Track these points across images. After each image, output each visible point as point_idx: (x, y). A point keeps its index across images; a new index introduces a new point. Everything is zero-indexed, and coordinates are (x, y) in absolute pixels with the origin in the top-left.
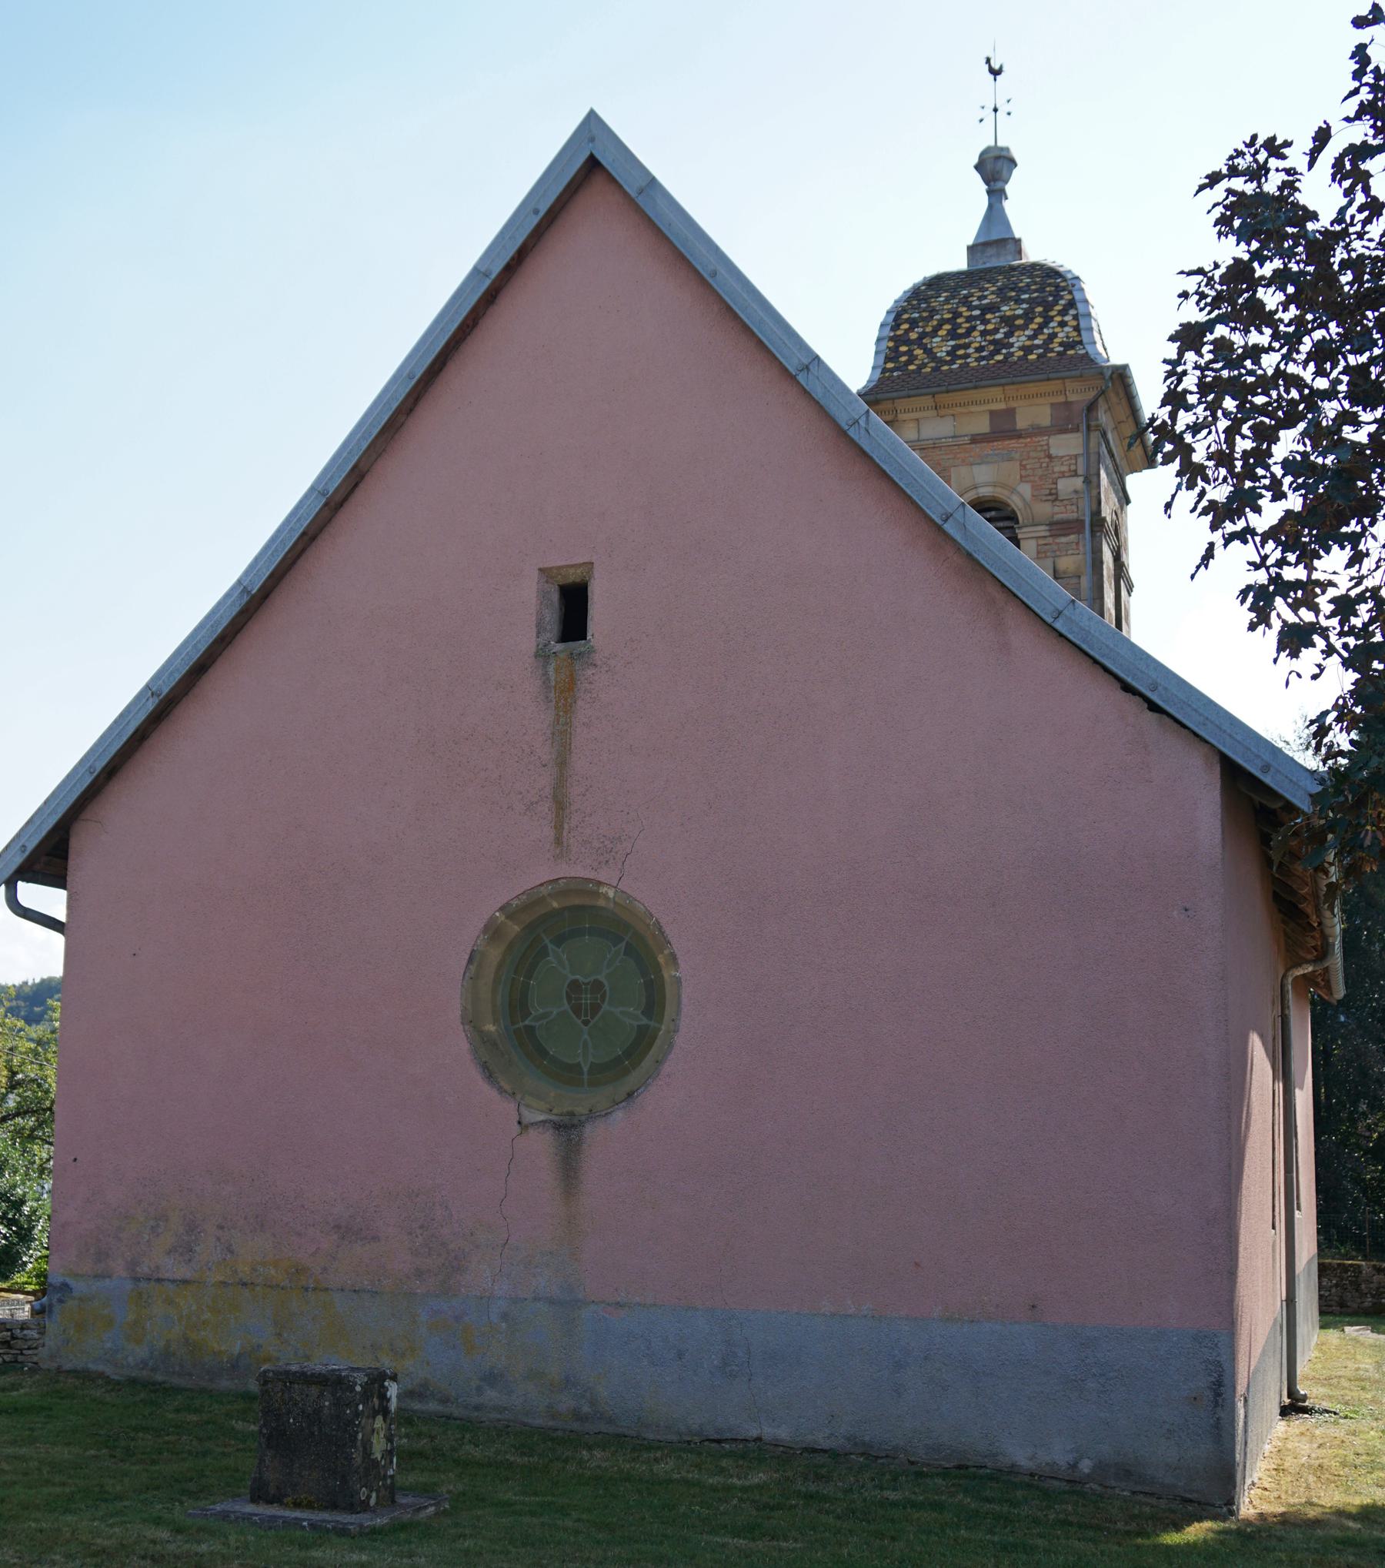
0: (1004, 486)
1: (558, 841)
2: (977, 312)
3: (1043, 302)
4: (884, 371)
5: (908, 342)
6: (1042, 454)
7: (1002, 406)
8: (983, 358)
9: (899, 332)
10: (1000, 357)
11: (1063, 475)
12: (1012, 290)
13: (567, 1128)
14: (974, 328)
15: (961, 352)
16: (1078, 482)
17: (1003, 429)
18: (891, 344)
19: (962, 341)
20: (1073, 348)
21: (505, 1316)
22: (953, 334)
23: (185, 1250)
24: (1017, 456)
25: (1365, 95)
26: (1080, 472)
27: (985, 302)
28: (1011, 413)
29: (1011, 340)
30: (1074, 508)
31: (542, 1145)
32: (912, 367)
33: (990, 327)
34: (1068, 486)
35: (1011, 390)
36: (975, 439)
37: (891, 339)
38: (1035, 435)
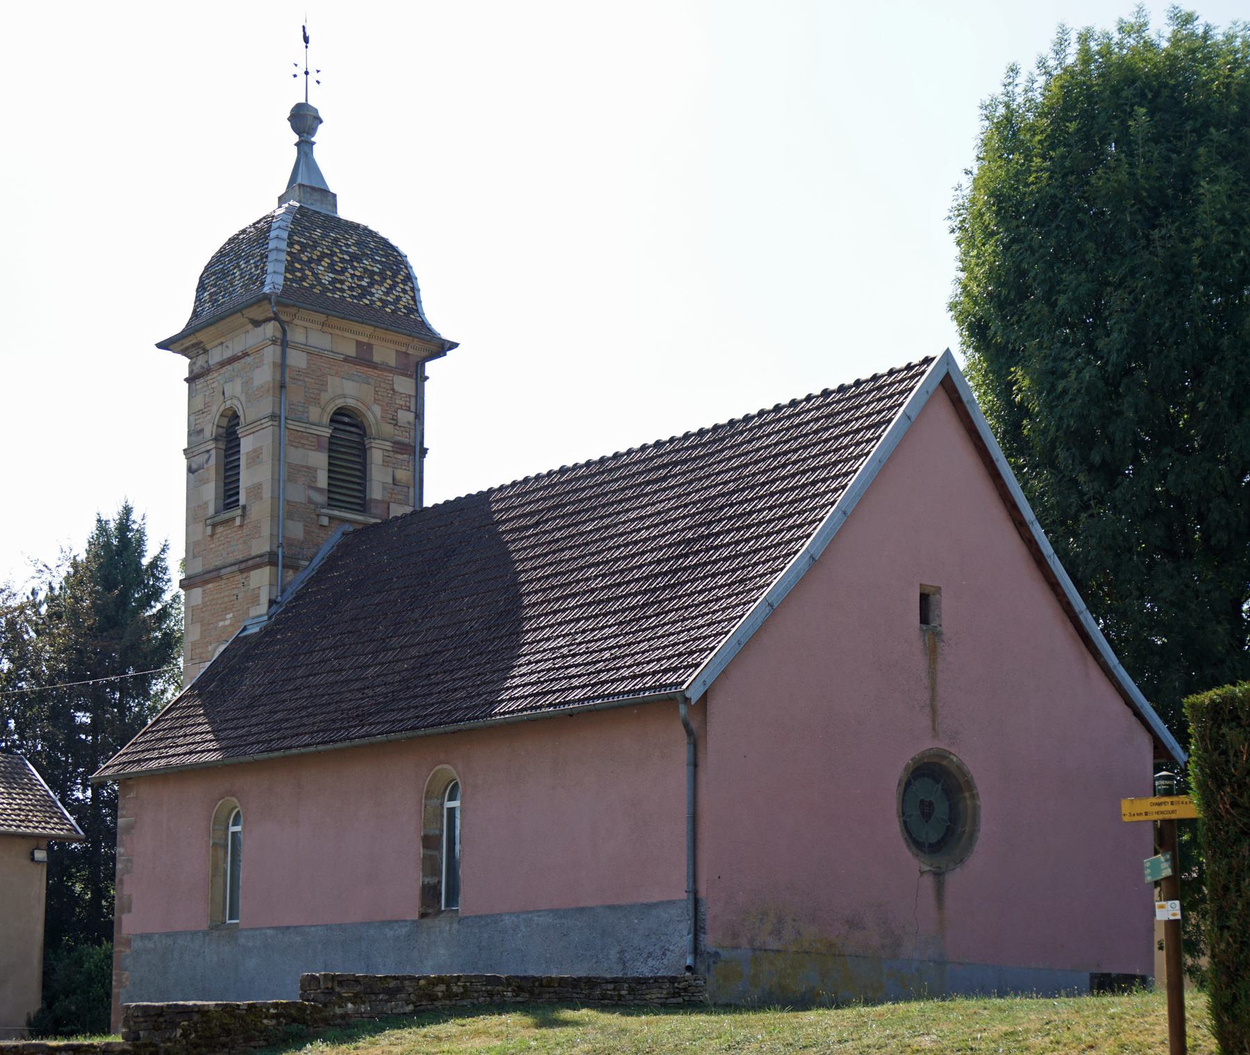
1: (934, 729)
4: (286, 279)
5: (300, 261)
7: (365, 340)
11: (401, 407)
13: (938, 875)
17: (363, 358)
21: (917, 970)
22: (331, 268)
23: (777, 932)
29: (373, 290)
31: (928, 881)
36: (347, 359)
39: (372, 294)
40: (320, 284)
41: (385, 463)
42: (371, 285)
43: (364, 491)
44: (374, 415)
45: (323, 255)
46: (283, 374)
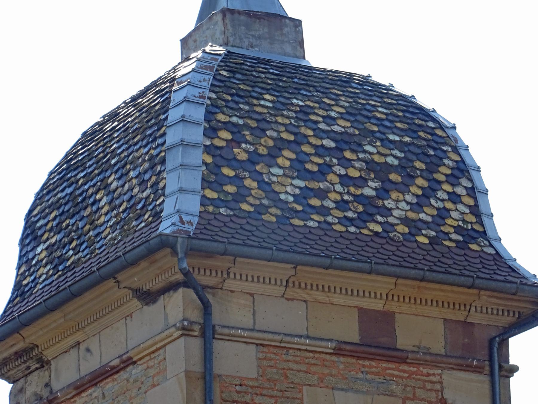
4: (205, 201)
5: (233, 162)
7: (378, 305)
19: (314, 185)
22: (298, 168)
29: (389, 203)
35: (407, 287)
36: (342, 349)
38: (426, 364)
40: (277, 202)
42: (383, 192)
45: (281, 144)
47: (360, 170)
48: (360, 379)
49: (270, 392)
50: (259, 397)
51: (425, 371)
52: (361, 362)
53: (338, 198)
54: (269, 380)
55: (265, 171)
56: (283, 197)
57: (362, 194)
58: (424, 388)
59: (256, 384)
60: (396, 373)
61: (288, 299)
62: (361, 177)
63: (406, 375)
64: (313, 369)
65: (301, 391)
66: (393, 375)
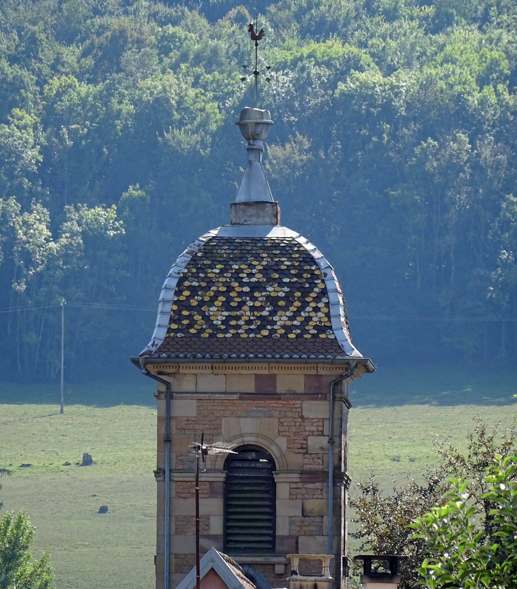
0: (266, 437)
2: (246, 289)
3: (301, 288)
4: (170, 330)
5: (189, 308)
6: (296, 415)
8: (252, 330)
9: (182, 298)
10: (265, 333)
11: (312, 433)
12: (276, 271)
14: (244, 303)
15: (233, 323)
16: (324, 441)
18: (175, 308)
19: (234, 314)
20: (324, 332)
22: (226, 306)
24: (276, 414)
25: (86, 82)
26: (326, 433)
27: (253, 280)
28: (273, 378)
29: (275, 319)
30: (320, 461)
32: (192, 331)
33: (258, 304)
34: (317, 443)
36: (244, 396)
37: (175, 303)
39: (274, 323)
40: (211, 325)
41: (292, 496)
42: (273, 313)
43: (273, 528)
44: (278, 447)
45: (218, 293)
46: (168, 426)
47: (262, 302)
48: (254, 411)
49: (204, 422)
50: (197, 425)
51: (292, 403)
52: (255, 402)
53: (247, 319)
54: (204, 417)
55: (206, 310)
56: (215, 322)
57: (261, 315)
58: (291, 411)
59: (196, 419)
60: (276, 405)
61: (215, 375)
62: (261, 306)
63: (281, 406)
64: (229, 408)
65: (221, 420)
66: (274, 407)
